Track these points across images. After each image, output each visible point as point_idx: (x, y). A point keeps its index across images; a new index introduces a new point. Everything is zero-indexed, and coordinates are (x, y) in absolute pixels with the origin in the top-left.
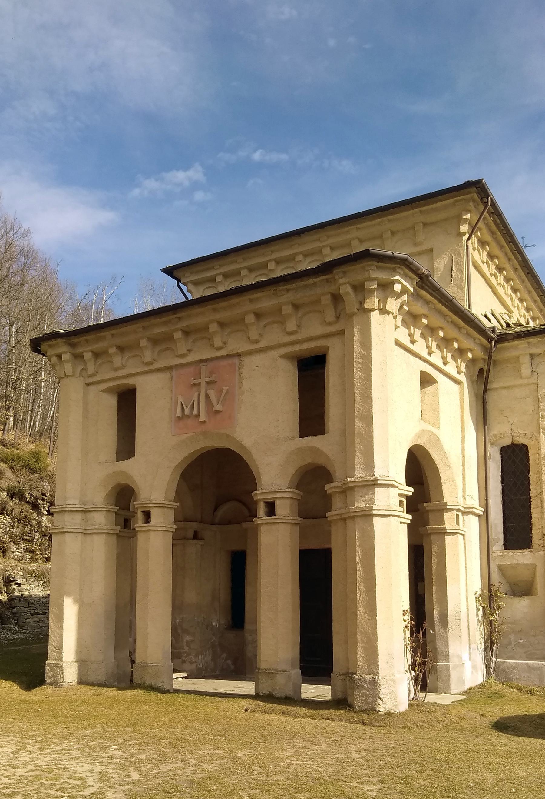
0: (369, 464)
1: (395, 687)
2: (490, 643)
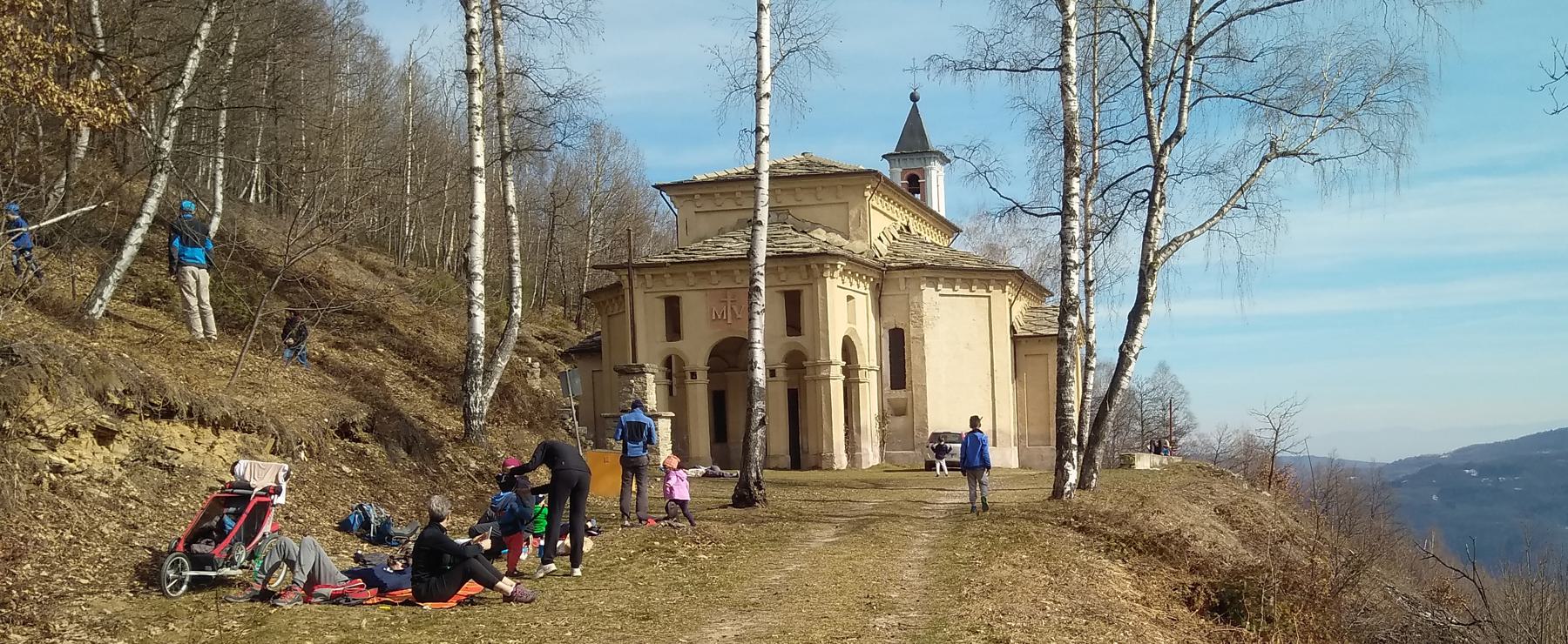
0: (828, 355)
1: (841, 460)
2: (883, 443)
